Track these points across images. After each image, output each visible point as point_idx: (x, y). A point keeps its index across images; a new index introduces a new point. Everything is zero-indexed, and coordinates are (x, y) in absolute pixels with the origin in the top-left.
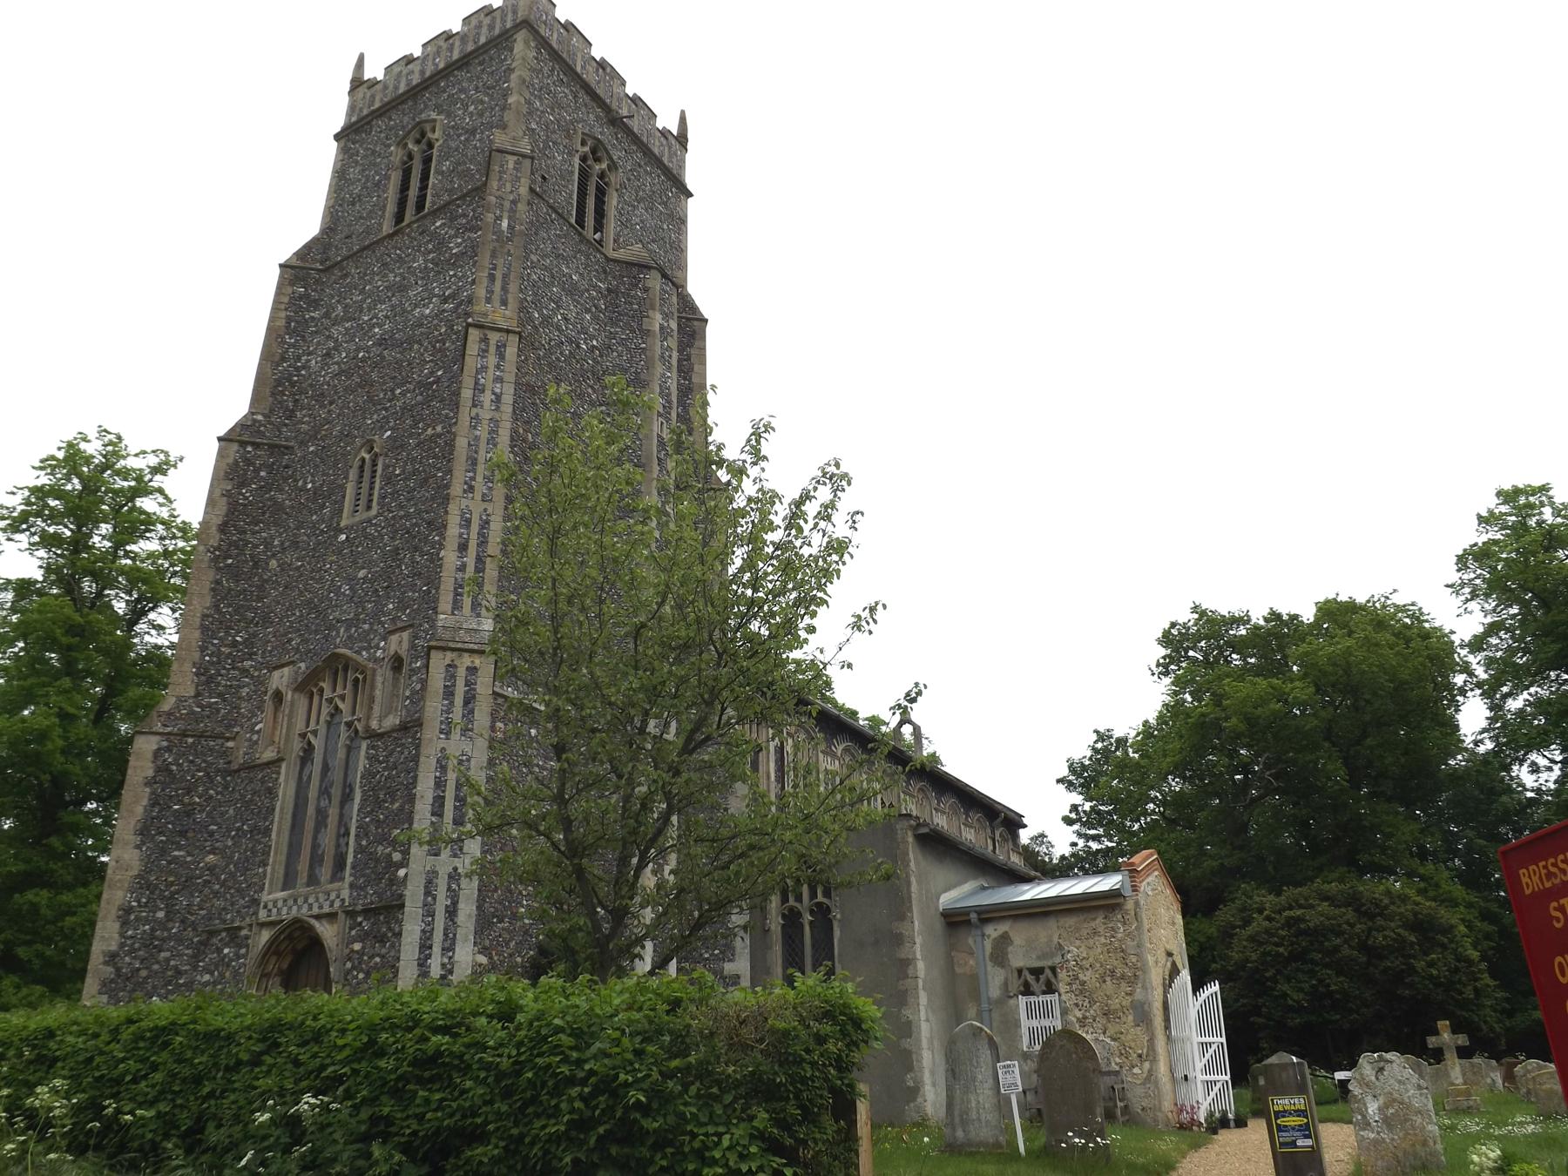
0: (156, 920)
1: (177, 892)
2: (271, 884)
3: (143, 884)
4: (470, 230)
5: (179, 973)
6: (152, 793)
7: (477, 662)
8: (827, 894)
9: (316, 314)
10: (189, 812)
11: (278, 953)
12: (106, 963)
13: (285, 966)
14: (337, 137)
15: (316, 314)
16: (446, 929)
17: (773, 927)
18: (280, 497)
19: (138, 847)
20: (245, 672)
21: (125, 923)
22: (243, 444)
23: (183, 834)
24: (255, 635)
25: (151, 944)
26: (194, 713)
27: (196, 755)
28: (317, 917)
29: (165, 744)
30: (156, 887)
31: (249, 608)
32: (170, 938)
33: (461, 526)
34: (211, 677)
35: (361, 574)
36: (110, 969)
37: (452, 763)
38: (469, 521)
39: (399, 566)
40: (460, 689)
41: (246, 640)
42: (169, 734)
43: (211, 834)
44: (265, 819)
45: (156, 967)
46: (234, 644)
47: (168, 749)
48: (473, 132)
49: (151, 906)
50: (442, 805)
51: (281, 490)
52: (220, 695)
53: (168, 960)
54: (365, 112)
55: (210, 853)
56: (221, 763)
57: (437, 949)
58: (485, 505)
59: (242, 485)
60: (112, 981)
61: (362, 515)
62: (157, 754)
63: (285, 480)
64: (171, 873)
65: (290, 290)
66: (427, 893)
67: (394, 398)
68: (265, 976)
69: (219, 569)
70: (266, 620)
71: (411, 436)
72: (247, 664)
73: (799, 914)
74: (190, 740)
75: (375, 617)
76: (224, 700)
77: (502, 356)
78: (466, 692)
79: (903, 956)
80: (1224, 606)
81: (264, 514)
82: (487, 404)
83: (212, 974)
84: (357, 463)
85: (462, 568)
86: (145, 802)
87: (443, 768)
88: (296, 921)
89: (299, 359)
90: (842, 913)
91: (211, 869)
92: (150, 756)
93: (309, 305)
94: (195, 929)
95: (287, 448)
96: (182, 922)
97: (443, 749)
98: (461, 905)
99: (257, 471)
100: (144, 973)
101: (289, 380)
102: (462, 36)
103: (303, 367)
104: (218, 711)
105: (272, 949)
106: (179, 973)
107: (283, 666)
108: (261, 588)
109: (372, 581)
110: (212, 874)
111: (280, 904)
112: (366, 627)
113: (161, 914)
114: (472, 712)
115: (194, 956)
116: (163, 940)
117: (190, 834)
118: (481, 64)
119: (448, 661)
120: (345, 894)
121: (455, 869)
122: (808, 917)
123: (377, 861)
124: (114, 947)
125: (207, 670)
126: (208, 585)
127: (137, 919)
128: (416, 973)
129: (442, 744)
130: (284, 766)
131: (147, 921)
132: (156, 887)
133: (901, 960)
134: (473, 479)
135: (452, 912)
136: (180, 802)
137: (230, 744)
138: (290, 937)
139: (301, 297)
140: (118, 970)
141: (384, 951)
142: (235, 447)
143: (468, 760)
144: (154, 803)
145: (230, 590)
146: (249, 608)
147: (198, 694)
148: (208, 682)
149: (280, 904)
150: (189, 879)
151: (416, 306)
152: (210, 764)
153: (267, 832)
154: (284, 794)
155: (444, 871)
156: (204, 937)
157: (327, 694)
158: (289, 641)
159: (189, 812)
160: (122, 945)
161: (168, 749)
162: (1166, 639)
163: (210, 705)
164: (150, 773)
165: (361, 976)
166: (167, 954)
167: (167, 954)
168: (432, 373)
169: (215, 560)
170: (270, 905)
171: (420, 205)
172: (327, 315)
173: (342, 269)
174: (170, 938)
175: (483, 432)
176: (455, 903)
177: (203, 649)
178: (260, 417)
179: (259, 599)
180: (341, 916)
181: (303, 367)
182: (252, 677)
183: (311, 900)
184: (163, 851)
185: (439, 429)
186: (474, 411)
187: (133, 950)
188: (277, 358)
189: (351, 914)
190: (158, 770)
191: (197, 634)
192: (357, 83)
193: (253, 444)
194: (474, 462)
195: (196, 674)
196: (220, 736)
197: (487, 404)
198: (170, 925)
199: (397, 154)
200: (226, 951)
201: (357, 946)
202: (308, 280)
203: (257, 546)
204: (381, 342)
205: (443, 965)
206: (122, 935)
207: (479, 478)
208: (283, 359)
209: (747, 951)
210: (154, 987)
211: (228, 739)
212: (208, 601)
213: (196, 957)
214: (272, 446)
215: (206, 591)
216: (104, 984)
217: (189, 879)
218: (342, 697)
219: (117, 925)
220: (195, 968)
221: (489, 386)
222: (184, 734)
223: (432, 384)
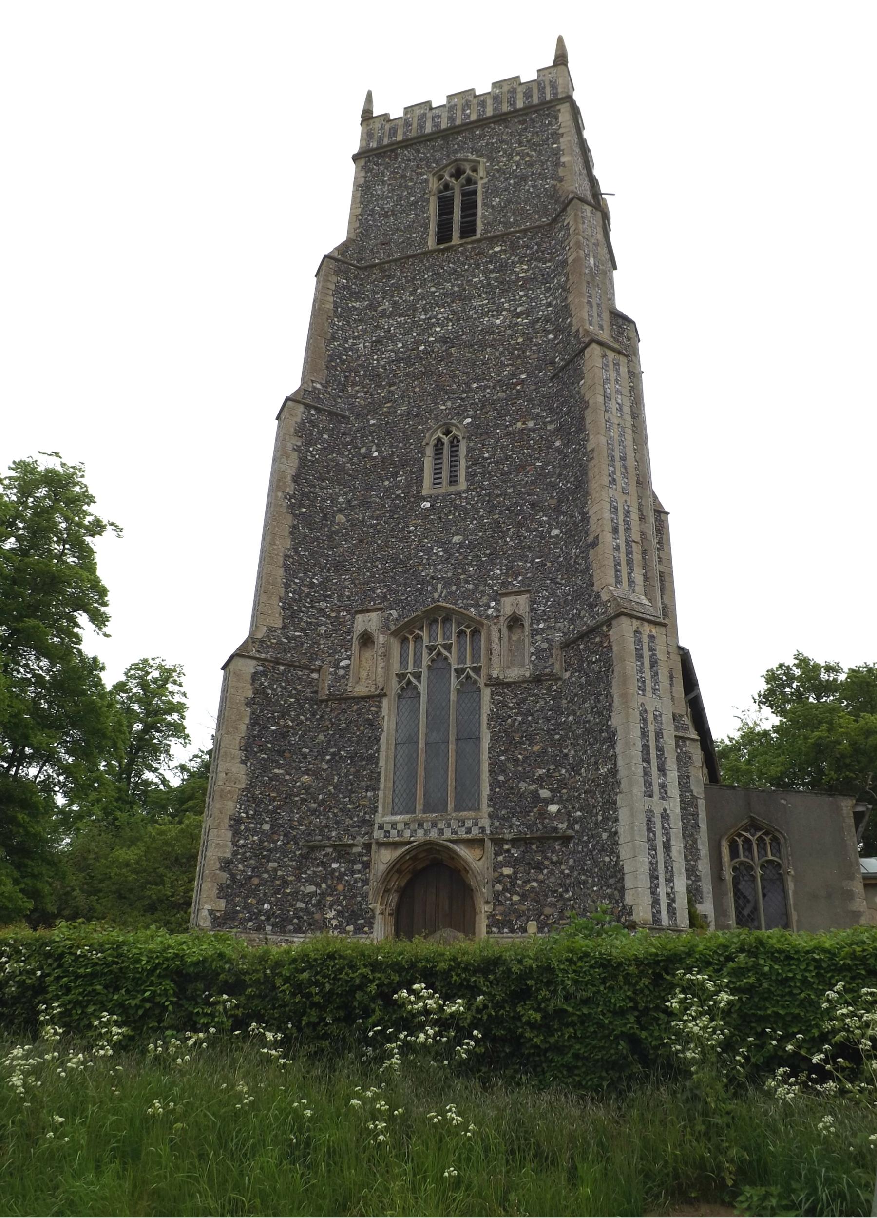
0: (263, 832)
1: (280, 807)
2: (384, 808)
3: (248, 797)
4: (538, 260)
5: (286, 883)
6: (253, 713)
7: (654, 632)
8: (777, 851)
9: (357, 305)
10: (283, 734)
11: (399, 872)
12: (221, 869)
13: (403, 884)
14: (355, 158)
15: (357, 305)
16: (665, 862)
17: (727, 878)
18: (341, 460)
19: (243, 762)
20: (321, 611)
21: (236, 833)
22: (307, 406)
23: (281, 753)
24: (328, 579)
25: (260, 854)
26: (281, 643)
27: (288, 682)
28: (471, 843)
29: (261, 668)
30: (261, 801)
31: (322, 555)
32: (276, 850)
33: (612, 512)
34: (294, 612)
35: (457, 539)
36: (226, 875)
37: (650, 717)
38: (616, 508)
39: (503, 538)
40: (646, 653)
41: (320, 583)
42: (265, 660)
43: (305, 756)
44: (368, 748)
45: (266, 876)
46: (312, 585)
47: (264, 674)
48: (524, 178)
49: (257, 817)
50: (648, 753)
51: (341, 454)
52: (302, 630)
53: (275, 870)
54: (386, 141)
55: (305, 773)
56: (308, 693)
57: (662, 880)
58: (625, 497)
59: (308, 444)
60: (228, 886)
61: (445, 488)
62: (255, 676)
63: (345, 445)
64: (274, 789)
65: (334, 279)
66: (649, 830)
67: (469, 390)
68: (387, 891)
69: (295, 516)
70: (339, 567)
71: (497, 426)
72: (323, 604)
73: (751, 868)
74: (282, 668)
75: (482, 578)
76: (306, 635)
77: (618, 371)
78: (651, 656)
79: (854, 909)
80: (819, 657)
81: (329, 472)
82: (614, 411)
83: (318, 885)
84: (433, 442)
85: (617, 548)
86: (247, 721)
87: (645, 720)
88: (429, 847)
89: (346, 341)
90: (795, 870)
91: (306, 788)
92: (249, 678)
93: (351, 296)
94: (296, 843)
95: (343, 417)
96: (285, 835)
97: (642, 705)
98: (673, 843)
99: (320, 433)
100: (256, 881)
101: (340, 358)
102: (481, 100)
103: (351, 349)
104: (302, 644)
105: (396, 868)
106: (286, 883)
107: (369, 611)
108: (330, 538)
109: (471, 547)
110: (307, 793)
111: (400, 827)
112: (471, 587)
113: (266, 827)
114: (656, 674)
115: (298, 868)
116: (270, 851)
117: (287, 755)
118: (520, 123)
119: (635, 628)
120: (485, 822)
121: (665, 810)
122: (759, 872)
123: (521, 796)
124: (228, 855)
125: (291, 606)
126: (288, 530)
127: (247, 829)
128: (651, 900)
129: (641, 699)
130: (385, 702)
131: (255, 832)
132: (261, 801)
133: (854, 912)
134: (614, 473)
135: (667, 847)
136: (277, 724)
137: (315, 676)
138: (414, 858)
139: (344, 287)
140: (233, 877)
141: (541, 877)
142: (301, 408)
143: (660, 716)
144: (254, 722)
145: (305, 536)
146: (322, 555)
147: (284, 627)
148: (293, 616)
149: (400, 827)
150: (289, 796)
151: (484, 315)
152: (299, 692)
153: (373, 759)
154: (388, 727)
155: (658, 811)
156: (305, 851)
157: (426, 642)
158: (373, 589)
159: (283, 734)
160: (235, 853)
161: (264, 674)
162: (771, 677)
163: (295, 638)
164: (250, 694)
165: (516, 898)
166: (275, 865)
167: (275, 865)
168: (514, 375)
169: (292, 506)
170: (387, 827)
171: (468, 229)
172: (372, 307)
173: (383, 270)
174: (276, 850)
175: (614, 433)
176: (669, 840)
177: (287, 586)
178: (319, 386)
179: (331, 548)
180: (488, 843)
181: (351, 349)
182: (329, 617)
183: (440, 825)
184: (265, 769)
185: (531, 424)
186: (607, 415)
187: (244, 859)
188: (329, 337)
189: (498, 842)
190: (256, 692)
191: (281, 572)
192: (367, 116)
193: (316, 408)
194: (613, 459)
195: (283, 608)
196: (306, 667)
197: (614, 411)
198: (276, 837)
199: (434, 185)
200: (335, 865)
201: (507, 871)
202: (346, 275)
203: (325, 500)
204: (444, 340)
205: (668, 894)
206: (235, 844)
207: (618, 473)
208: (334, 338)
209: (711, 895)
210: (265, 894)
211: (313, 671)
212: (289, 543)
213: (299, 869)
214: (331, 413)
215: (287, 534)
216: (221, 889)
217: (289, 796)
218: (448, 647)
219: (229, 834)
220: (299, 879)
221: (614, 396)
222: (277, 662)
223: (517, 384)
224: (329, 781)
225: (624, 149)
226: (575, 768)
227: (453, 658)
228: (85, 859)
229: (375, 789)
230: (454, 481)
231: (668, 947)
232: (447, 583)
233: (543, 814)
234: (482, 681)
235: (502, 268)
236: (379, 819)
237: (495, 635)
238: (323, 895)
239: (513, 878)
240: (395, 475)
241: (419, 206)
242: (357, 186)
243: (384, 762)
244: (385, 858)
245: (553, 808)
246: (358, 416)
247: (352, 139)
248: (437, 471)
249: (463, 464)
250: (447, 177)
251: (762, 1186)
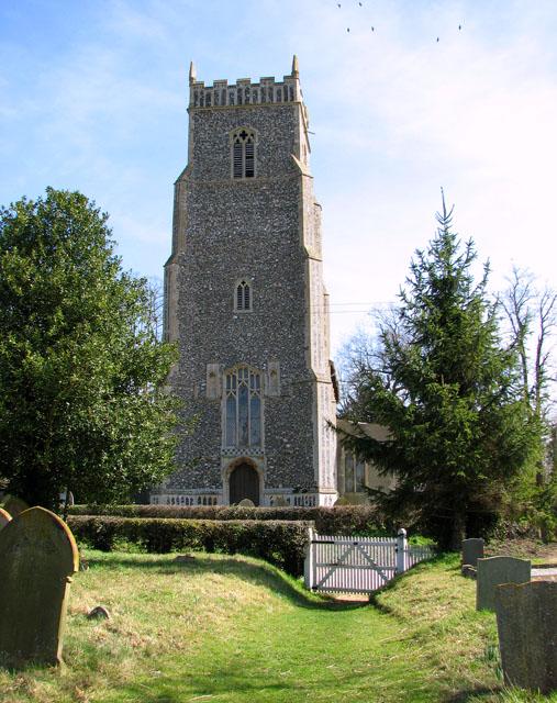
120: (263, 450)
204: (240, 234)
224: (201, 432)
225: (305, 92)
226: (297, 432)
227: (249, 386)
228: (487, 380)
229: (220, 436)
230: (247, 307)
231: (190, 652)
232: (246, 354)
233: (285, 448)
234: (260, 397)
235: (268, 199)
236: (222, 448)
237: (266, 379)
238: (202, 475)
239: (274, 470)
240: (220, 301)
241: (225, 151)
242: (191, 130)
243: (224, 427)
244: (225, 462)
245: (288, 446)
246: (201, 267)
247: (184, 99)
248: (240, 301)
249: (251, 301)
250: (238, 137)
251: (391, 430)
